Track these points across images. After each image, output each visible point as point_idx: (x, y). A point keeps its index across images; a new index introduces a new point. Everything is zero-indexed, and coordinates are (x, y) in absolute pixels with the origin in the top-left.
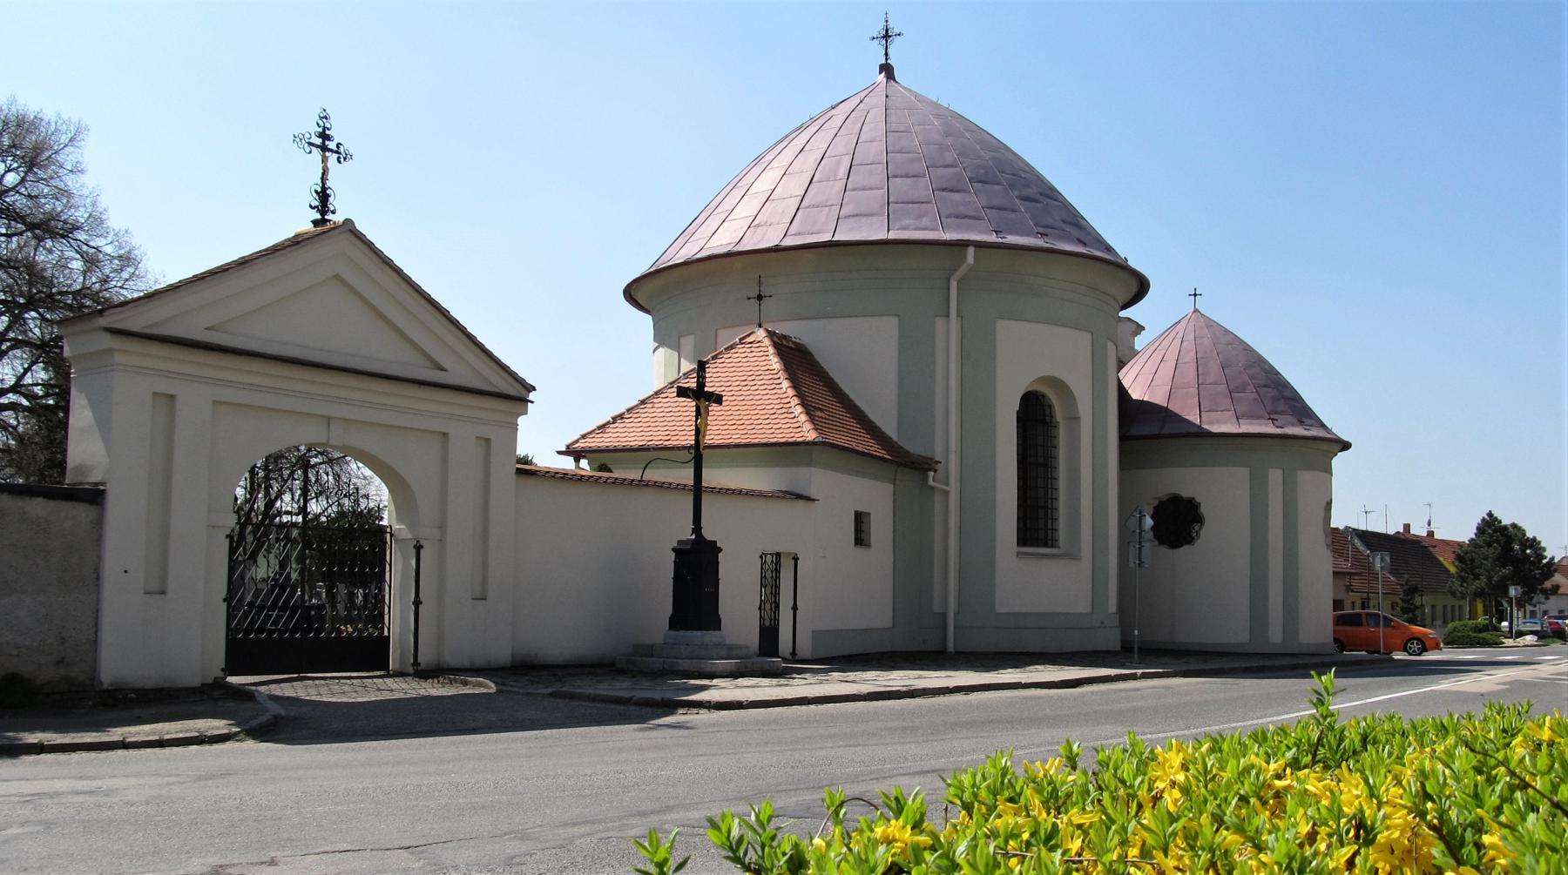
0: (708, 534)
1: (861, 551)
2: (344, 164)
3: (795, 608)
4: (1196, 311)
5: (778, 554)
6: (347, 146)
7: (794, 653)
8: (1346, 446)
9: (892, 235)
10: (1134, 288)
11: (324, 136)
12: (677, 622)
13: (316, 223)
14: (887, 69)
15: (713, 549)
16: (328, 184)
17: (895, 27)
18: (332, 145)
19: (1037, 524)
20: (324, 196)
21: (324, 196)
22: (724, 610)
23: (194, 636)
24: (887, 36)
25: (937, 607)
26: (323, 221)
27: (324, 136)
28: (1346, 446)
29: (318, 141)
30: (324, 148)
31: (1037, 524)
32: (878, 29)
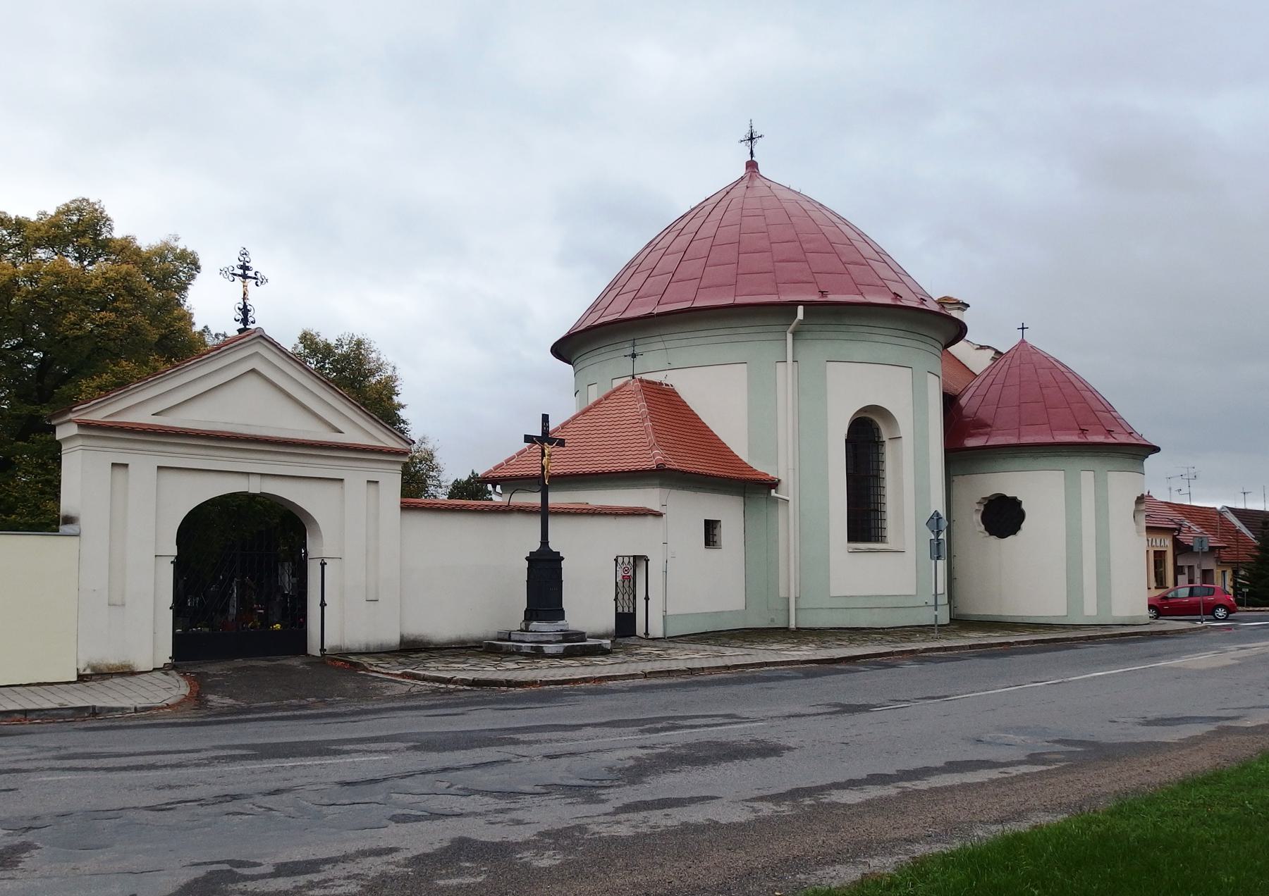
0: (553, 546)
1: (712, 552)
2: (261, 287)
3: (647, 599)
4: (1023, 341)
5: (634, 557)
6: (263, 272)
7: (647, 633)
8: (1156, 449)
9: (739, 300)
10: (954, 331)
11: (245, 267)
12: (530, 615)
13: (240, 331)
14: (752, 165)
15: (557, 559)
16: (248, 302)
17: (758, 131)
18: (250, 273)
19: (865, 522)
20: (245, 311)
21: (245, 311)
22: (566, 605)
23: (1179, 564)
24: (751, 139)
25: (782, 594)
26: (245, 330)
27: (245, 267)
28: (1156, 449)
29: (240, 272)
30: (245, 277)
31: (865, 522)
32: (745, 133)
